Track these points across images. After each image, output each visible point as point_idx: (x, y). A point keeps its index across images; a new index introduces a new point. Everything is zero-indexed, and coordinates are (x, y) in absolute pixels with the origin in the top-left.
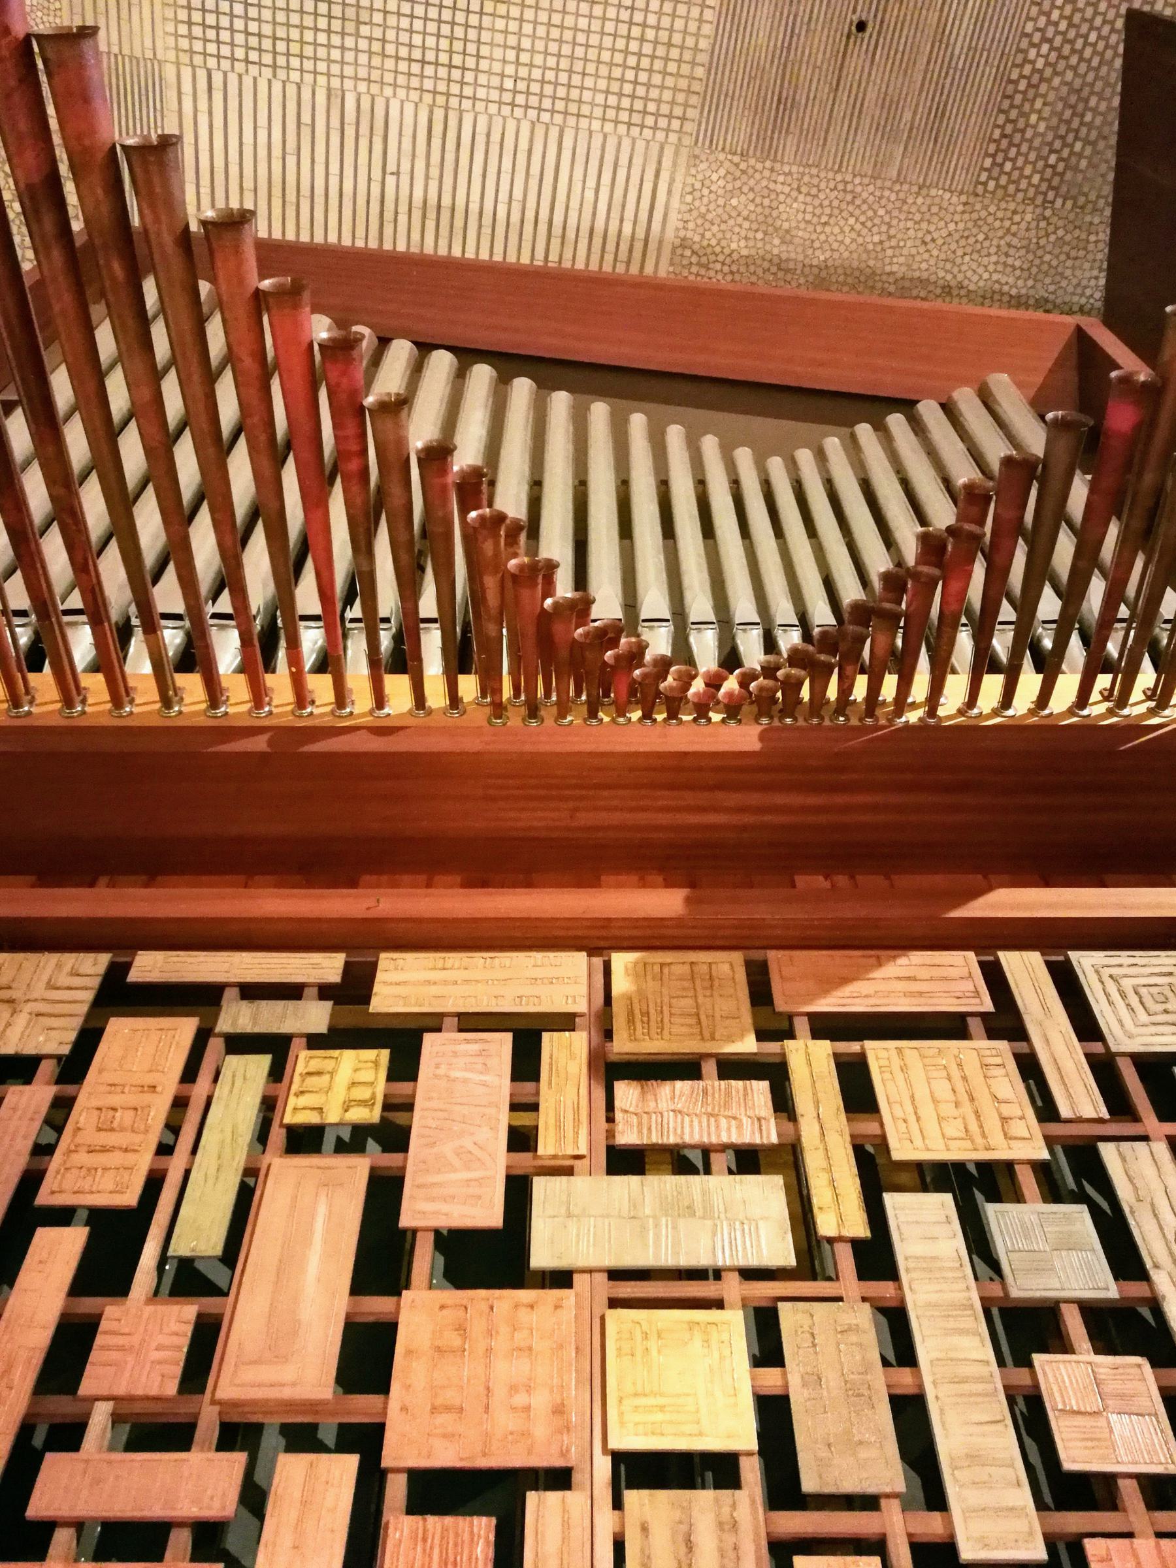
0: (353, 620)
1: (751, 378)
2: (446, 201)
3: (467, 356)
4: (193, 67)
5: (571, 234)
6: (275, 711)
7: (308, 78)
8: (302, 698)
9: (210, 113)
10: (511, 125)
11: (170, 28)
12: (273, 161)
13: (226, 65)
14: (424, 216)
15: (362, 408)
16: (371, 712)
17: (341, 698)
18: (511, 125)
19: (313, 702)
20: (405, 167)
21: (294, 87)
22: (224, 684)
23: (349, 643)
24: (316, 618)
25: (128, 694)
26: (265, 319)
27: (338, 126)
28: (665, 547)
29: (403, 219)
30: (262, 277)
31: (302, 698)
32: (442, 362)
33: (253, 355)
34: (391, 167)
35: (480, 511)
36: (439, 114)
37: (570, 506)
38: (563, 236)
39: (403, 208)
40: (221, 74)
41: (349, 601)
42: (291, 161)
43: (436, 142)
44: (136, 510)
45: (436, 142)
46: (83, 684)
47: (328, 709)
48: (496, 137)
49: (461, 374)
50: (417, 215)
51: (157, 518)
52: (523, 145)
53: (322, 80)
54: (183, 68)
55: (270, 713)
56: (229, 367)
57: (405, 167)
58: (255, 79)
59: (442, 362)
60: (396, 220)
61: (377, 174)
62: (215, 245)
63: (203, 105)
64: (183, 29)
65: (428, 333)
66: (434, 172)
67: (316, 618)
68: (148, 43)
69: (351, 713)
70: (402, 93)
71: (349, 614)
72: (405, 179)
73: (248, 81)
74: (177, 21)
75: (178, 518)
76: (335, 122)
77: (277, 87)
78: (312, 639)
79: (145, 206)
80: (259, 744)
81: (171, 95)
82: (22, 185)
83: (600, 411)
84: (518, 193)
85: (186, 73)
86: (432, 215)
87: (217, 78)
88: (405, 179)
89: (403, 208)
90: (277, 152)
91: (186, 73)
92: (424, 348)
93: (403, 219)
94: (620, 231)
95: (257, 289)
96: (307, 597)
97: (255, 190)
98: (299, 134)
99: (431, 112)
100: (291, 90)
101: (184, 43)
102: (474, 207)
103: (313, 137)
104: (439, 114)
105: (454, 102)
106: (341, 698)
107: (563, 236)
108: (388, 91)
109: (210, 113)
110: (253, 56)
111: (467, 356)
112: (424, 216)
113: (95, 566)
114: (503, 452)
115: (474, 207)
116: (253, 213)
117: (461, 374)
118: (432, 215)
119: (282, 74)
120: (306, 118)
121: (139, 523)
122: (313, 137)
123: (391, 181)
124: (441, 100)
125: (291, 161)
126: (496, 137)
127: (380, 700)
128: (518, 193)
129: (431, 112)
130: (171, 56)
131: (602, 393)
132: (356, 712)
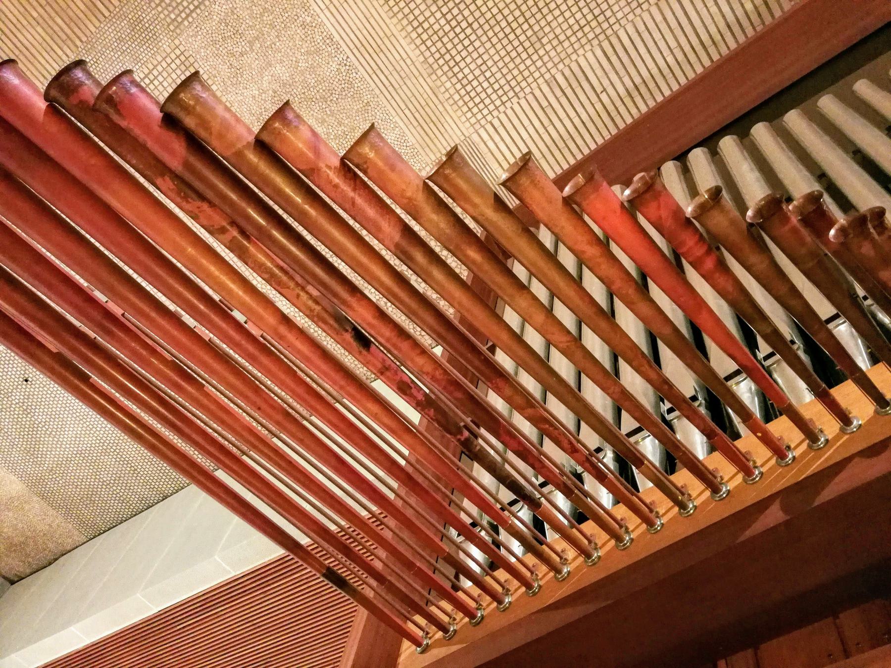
0: (766, 358)
1: (804, 73)
2: (638, 80)
3: (710, 142)
4: (483, 127)
5: (717, 38)
6: (763, 470)
7: (534, 85)
8: (779, 450)
9: (503, 140)
10: (646, 16)
11: (463, 119)
12: (543, 136)
13: (495, 113)
14: (632, 98)
15: (688, 221)
16: (842, 431)
17: (810, 433)
18: (646, 16)
19: (789, 447)
20: (606, 83)
21: (531, 95)
22: (711, 467)
23: (775, 376)
24: (737, 373)
25: (651, 511)
26: (586, 218)
27: (561, 93)
28: (819, 167)
29: (622, 109)
30: (562, 189)
31: (779, 450)
32: (728, 145)
33: (590, 243)
34: (599, 89)
35: (836, 226)
36: (606, 44)
37: (866, 176)
38: (714, 43)
39: (618, 103)
40: (496, 119)
41: (753, 346)
42: (551, 129)
43: (614, 59)
44: (584, 342)
45: (614, 59)
46: (619, 517)
47: (804, 446)
48: (641, 28)
49: (714, 153)
50: (627, 100)
51: (598, 391)
52: (659, 18)
53: (541, 81)
54: (480, 131)
55: (762, 474)
56: (584, 267)
57: (606, 83)
58: (512, 108)
59: (698, 158)
60: (619, 113)
61: (594, 99)
62: (519, 192)
63: (497, 138)
64: (469, 115)
65: (677, 149)
66: (622, 72)
67: (737, 373)
68: (459, 133)
69: (827, 441)
70: (581, 52)
71: (761, 355)
72: (610, 90)
73: (509, 112)
74: (464, 114)
75: (609, 380)
76: (559, 93)
77: (523, 102)
78: (745, 390)
79: (462, 203)
80: (775, 516)
81: (482, 146)
82: (393, 249)
83: (794, 119)
84: (673, 44)
85: (482, 132)
86: (635, 94)
87: (496, 123)
88: (610, 90)
89: (618, 103)
90: (541, 130)
91: (482, 132)
92: (681, 158)
93: (622, 109)
94: (746, 13)
95: (564, 198)
96: (721, 363)
97: (544, 156)
98: (546, 114)
99: (601, 47)
100: (530, 97)
101: (473, 120)
102: (655, 71)
103: (553, 109)
104: (606, 44)
105: (609, 32)
106: (810, 433)
107: (714, 43)
108: (574, 57)
109: (503, 140)
110: (504, 98)
111: (710, 142)
112: (632, 98)
113: (579, 441)
114: (781, 176)
115: (655, 71)
116: (530, 153)
117: (714, 153)
118: (635, 94)
119: (521, 95)
120: (545, 104)
121: (589, 347)
122: (553, 109)
123: (604, 97)
124: (602, 37)
125: (551, 129)
126: (641, 28)
127: (844, 418)
128: (673, 44)
129: (601, 47)
130: (472, 130)
131: (818, 91)
132: (830, 437)
